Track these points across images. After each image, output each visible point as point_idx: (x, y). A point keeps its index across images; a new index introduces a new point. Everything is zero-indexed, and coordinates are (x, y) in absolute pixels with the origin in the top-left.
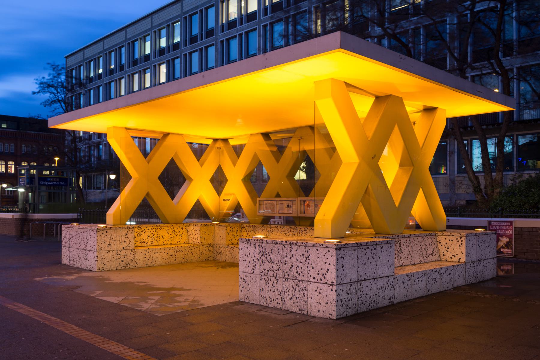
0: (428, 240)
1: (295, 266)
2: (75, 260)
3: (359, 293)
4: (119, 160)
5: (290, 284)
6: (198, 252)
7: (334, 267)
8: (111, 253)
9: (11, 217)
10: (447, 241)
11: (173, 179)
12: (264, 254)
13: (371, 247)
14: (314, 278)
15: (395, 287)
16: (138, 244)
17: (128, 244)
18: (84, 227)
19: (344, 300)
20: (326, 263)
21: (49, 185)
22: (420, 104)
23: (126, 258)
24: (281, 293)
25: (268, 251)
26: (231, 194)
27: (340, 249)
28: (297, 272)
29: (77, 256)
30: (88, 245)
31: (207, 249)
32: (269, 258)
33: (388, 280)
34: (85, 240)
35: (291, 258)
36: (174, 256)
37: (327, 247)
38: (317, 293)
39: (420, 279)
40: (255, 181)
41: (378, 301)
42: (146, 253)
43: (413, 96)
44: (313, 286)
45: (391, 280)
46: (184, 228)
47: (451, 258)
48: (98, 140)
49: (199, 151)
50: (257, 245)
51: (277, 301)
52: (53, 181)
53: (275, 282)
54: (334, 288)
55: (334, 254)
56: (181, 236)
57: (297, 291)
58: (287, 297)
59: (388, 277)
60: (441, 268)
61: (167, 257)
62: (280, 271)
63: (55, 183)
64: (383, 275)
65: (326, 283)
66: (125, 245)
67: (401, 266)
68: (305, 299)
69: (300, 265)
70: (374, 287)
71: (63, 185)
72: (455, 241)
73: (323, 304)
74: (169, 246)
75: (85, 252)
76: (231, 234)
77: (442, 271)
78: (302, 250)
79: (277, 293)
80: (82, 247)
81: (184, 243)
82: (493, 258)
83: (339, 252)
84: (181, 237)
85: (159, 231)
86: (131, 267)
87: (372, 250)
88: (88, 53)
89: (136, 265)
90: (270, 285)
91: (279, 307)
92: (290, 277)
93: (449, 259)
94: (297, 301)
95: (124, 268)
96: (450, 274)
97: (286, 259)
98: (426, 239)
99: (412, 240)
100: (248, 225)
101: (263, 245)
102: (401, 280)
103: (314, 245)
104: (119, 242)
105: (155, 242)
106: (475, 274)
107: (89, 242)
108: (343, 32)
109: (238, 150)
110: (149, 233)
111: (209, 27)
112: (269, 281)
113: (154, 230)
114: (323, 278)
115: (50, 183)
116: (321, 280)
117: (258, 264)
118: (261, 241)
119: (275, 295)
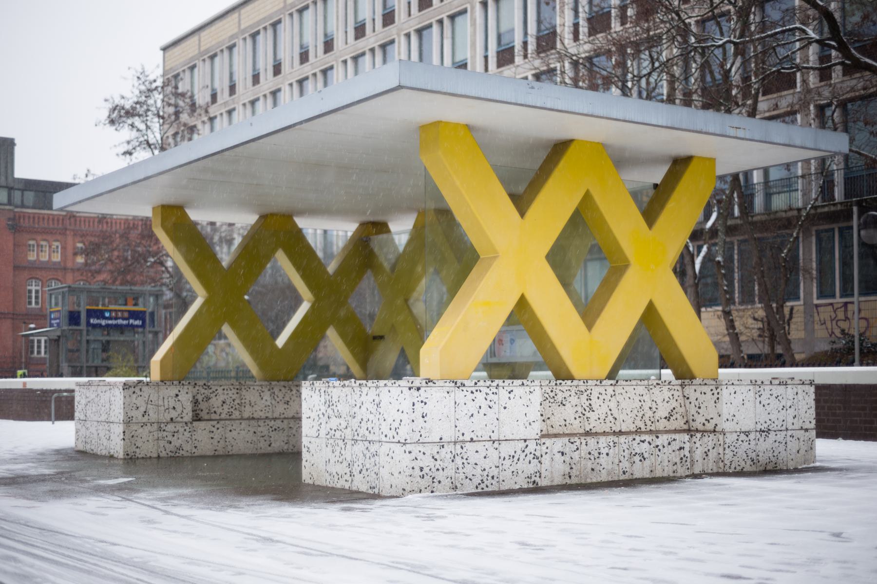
1: (365, 420)
2: (93, 442)
3: (458, 461)
5: (360, 447)
9: (21, 387)
10: (698, 394)
15: (543, 460)
17: (180, 412)
19: (426, 470)
21: (108, 326)
23: (175, 438)
25: (335, 399)
29: (95, 436)
30: (112, 414)
33: (524, 445)
34: (107, 406)
41: (501, 478)
42: (214, 429)
44: (385, 448)
47: (704, 424)
52: (116, 318)
53: (343, 447)
56: (287, 403)
57: (367, 459)
61: (255, 439)
62: (349, 429)
63: (120, 322)
65: (399, 442)
66: (174, 414)
68: (376, 469)
69: (371, 417)
70: (493, 455)
71: (137, 326)
72: (709, 393)
73: (396, 474)
75: (107, 425)
79: (345, 464)
80: (103, 418)
84: (286, 406)
86: (185, 454)
87: (487, 394)
88: (209, 39)
89: (194, 450)
90: (337, 453)
92: (359, 438)
94: (368, 473)
95: (172, 455)
97: (356, 409)
101: (330, 390)
104: (163, 408)
106: (754, 455)
107: (113, 407)
110: (226, 397)
111: (360, 18)
112: (336, 447)
113: (235, 391)
115: (110, 322)
117: (324, 420)
119: (342, 469)
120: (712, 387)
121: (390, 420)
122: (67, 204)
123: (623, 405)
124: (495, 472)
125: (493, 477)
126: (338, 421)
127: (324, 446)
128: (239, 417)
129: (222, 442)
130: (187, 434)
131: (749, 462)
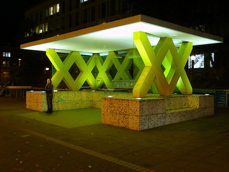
0: (183, 99)
3: (149, 120)
4: (51, 63)
5: (122, 116)
6: (86, 104)
7: (139, 109)
10: (191, 99)
11: (75, 71)
12: (112, 104)
13: (155, 101)
14: (131, 114)
16: (59, 100)
18: (37, 93)
20: (136, 107)
22: (180, 41)
24: (118, 120)
25: (113, 103)
26: (101, 78)
27: (141, 102)
28: (124, 111)
30: (38, 100)
31: (90, 102)
35: (122, 105)
37: (136, 101)
38: (132, 120)
40: (112, 72)
43: (175, 38)
45: (164, 115)
46: (80, 93)
47: (193, 106)
48: (43, 54)
49: (86, 58)
50: (109, 100)
51: (117, 123)
53: (116, 115)
54: (139, 117)
55: (139, 104)
58: (120, 121)
59: (163, 114)
60: (187, 111)
62: (118, 111)
64: (160, 113)
67: (170, 109)
72: (195, 99)
73: (135, 124)
74: (73, 101)
76: (100, 95)
77: (187, 112)
78: (126, 102)
79: (116, 120)
80: (35, 101)
81: (80, 100)
82: (213, 107)
83: (141, 103)
85: (68, 94)
90: (114, 117)
91: (117, 125)
93: (192, 107)
96: (191, 113)
97: (120, 106)
98: (182, 98)
99: (176, 98)
100: (108, 92)
102: (168, 115)
103: (131, 100)
105: (67, 100)
106: (204, 114)
108: (143, 16)
109: (104, 58)
114: (134, 114)
116: (134, 114)
118: (110, 99)
120: (195, 98)
121: (133, 110)
122: (80, 51)
123: (176, 102)
124: (156, 122)
125: (156, 123)
126: (114, 108)
127: (109, 114)
128: (68, 100)
129: (65, 107)
130: (57, 105)
131: (203, 115)
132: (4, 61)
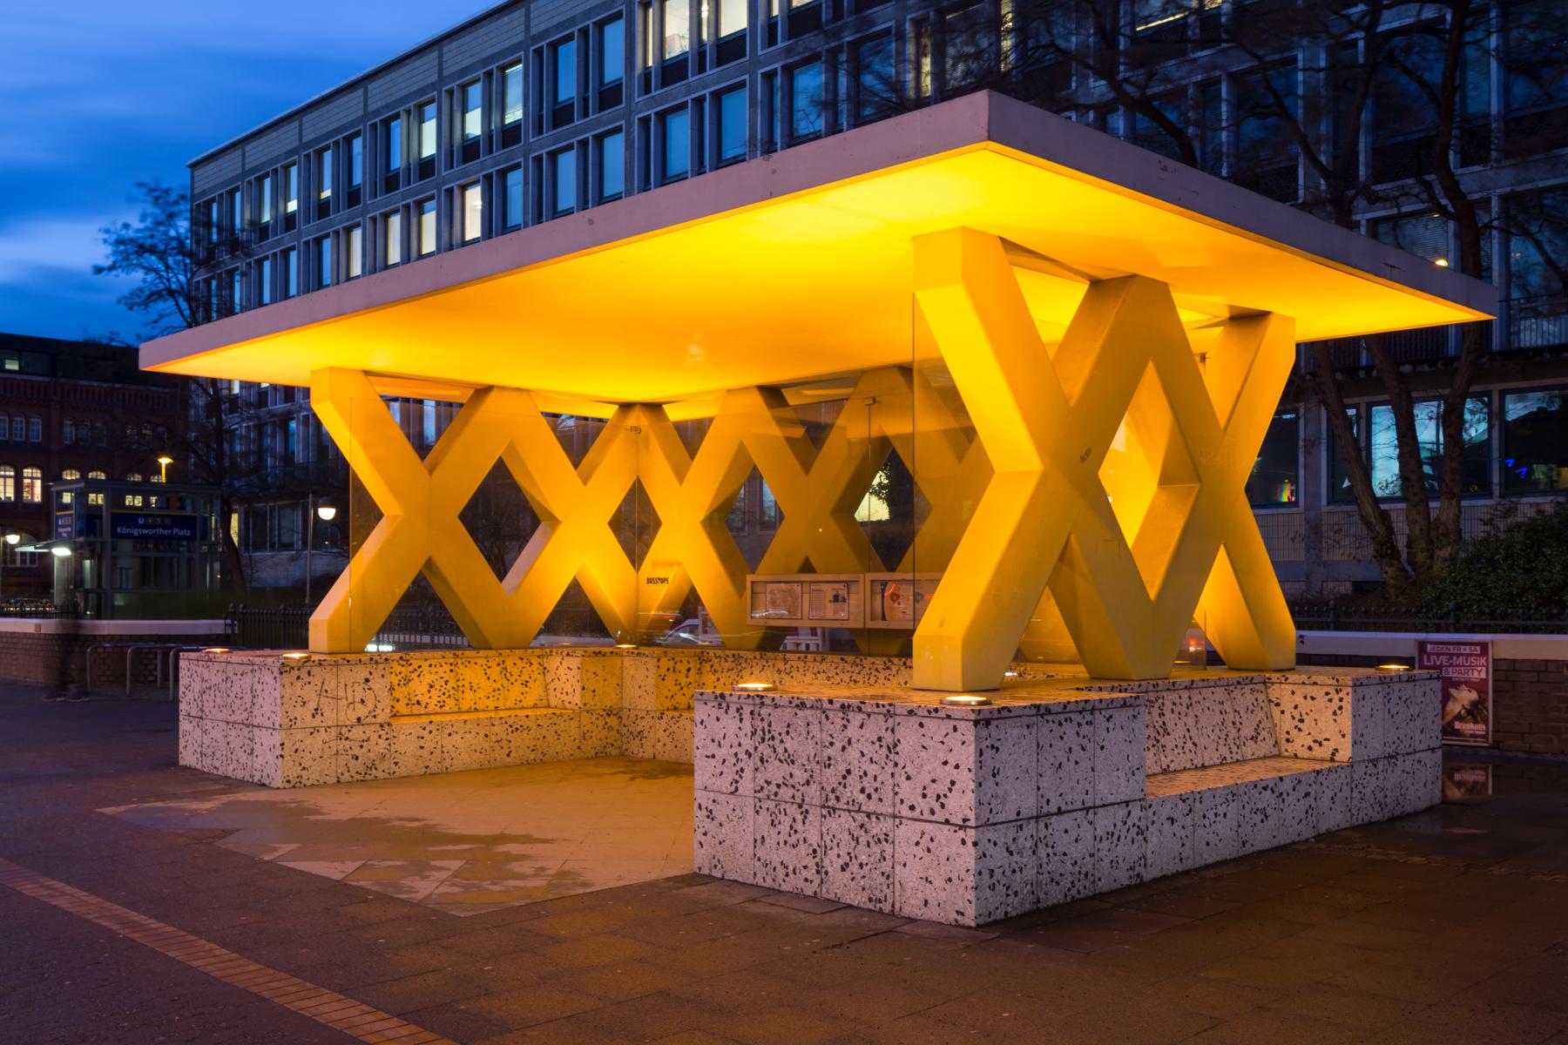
0: (1244, 698)
1: (856, 772)
2: (218, 754)
3: (1042, 851)
4: (346, 465)
5: (842, 823)
6: (575, 732)
7: (971, 775)
8: (323, 735)
9: (32, 630)
10: (1298, 699)
11: (502, 519)
12: (765, 736)
13: (1077, 718)
14: (912, 808)
15: (1148, 834)
16: (401, 708)
17: (371, 707)
18: (245, 660)
19: (998, 872)
20: (945, 763)
21: (141, 536)
22: (1219, 303)
23: (365, 750)
24: (815, 851)
25: (778, 728)
26: (671, 564)
27: (988, 723)
28: (863, 791)
29: (223, 743)
30: (256, 711)
31: (601, 723)
32: (780, 750)
33: (1125, 811)
34: (248, 698)
35: (844, 748)
36: (504, 743)
37: (949, 717)
38: (919, 851)
39: (1221, 811)
40: (740, 525)
41: (1097, 875)
42: (425, 733)
43: (1198, 278)
44: (908, 831)
45: (1136, 812)
46: (535, 661)
47: (1310, 748)
48: (284, 405)
49: (579, 439)
50: (747, 710)
51: (805, 873)
52: (154, 527)
53: (799, 818)
54: (971, 835)
55: (970, 737)
56: (526, 684)
57: (862, 846)
58: (832, 863)
59: (1127, 803)
60: (1281, 779)
61: (486, 745)
62: (814, 787)
63: (160, 531)
64: (1111, 799)
65: (947, 822)
66: (362, 711)
67: (1165, 772)
68: (886, 867)
69: (873, 770)
70: (1087, 833)
71: (184, 537)
72: (1322, 700)
73: (939, 882)
74: (492, 714)
75: (246, 730)
76: (671, 678)
77: (1283, 787)
78: (876, 726)
79: (803, 849)
80: (239, 716)
81: (535, 706)
82: (1433, 750)
83: (984, 733)
84: (524, 689)
85: (461, 669)
86: (381, 775)
87: (1080, 725)
88: (256, 154)
89: (394, 768)
90: (785, 827)
91: (809, 890)
92: (841, 805)
93: (1303, 753)
94: (862, 872)
95: (360, 777)
96: (1307, 794)
97: (830, 751)
98: (1237, 693)
99: (1196, 696)
100: (719, 652)
101: (764, 711)
102: (1165, 812)
103: (911, 712)
104: (344, 702)
105: (451, 703)
106: (1380, 796)
107: (259, 701)
108: (996, 94)
109: (691, 436)
110: (434, 677)
112: (782, 817)
113: (447, 668)
114: (937, 808)
115: (145, 531)
116: (932, 812)
117: (749, 765)
118: (758, 701)
119: (798, 857)
132: (105, 499)
